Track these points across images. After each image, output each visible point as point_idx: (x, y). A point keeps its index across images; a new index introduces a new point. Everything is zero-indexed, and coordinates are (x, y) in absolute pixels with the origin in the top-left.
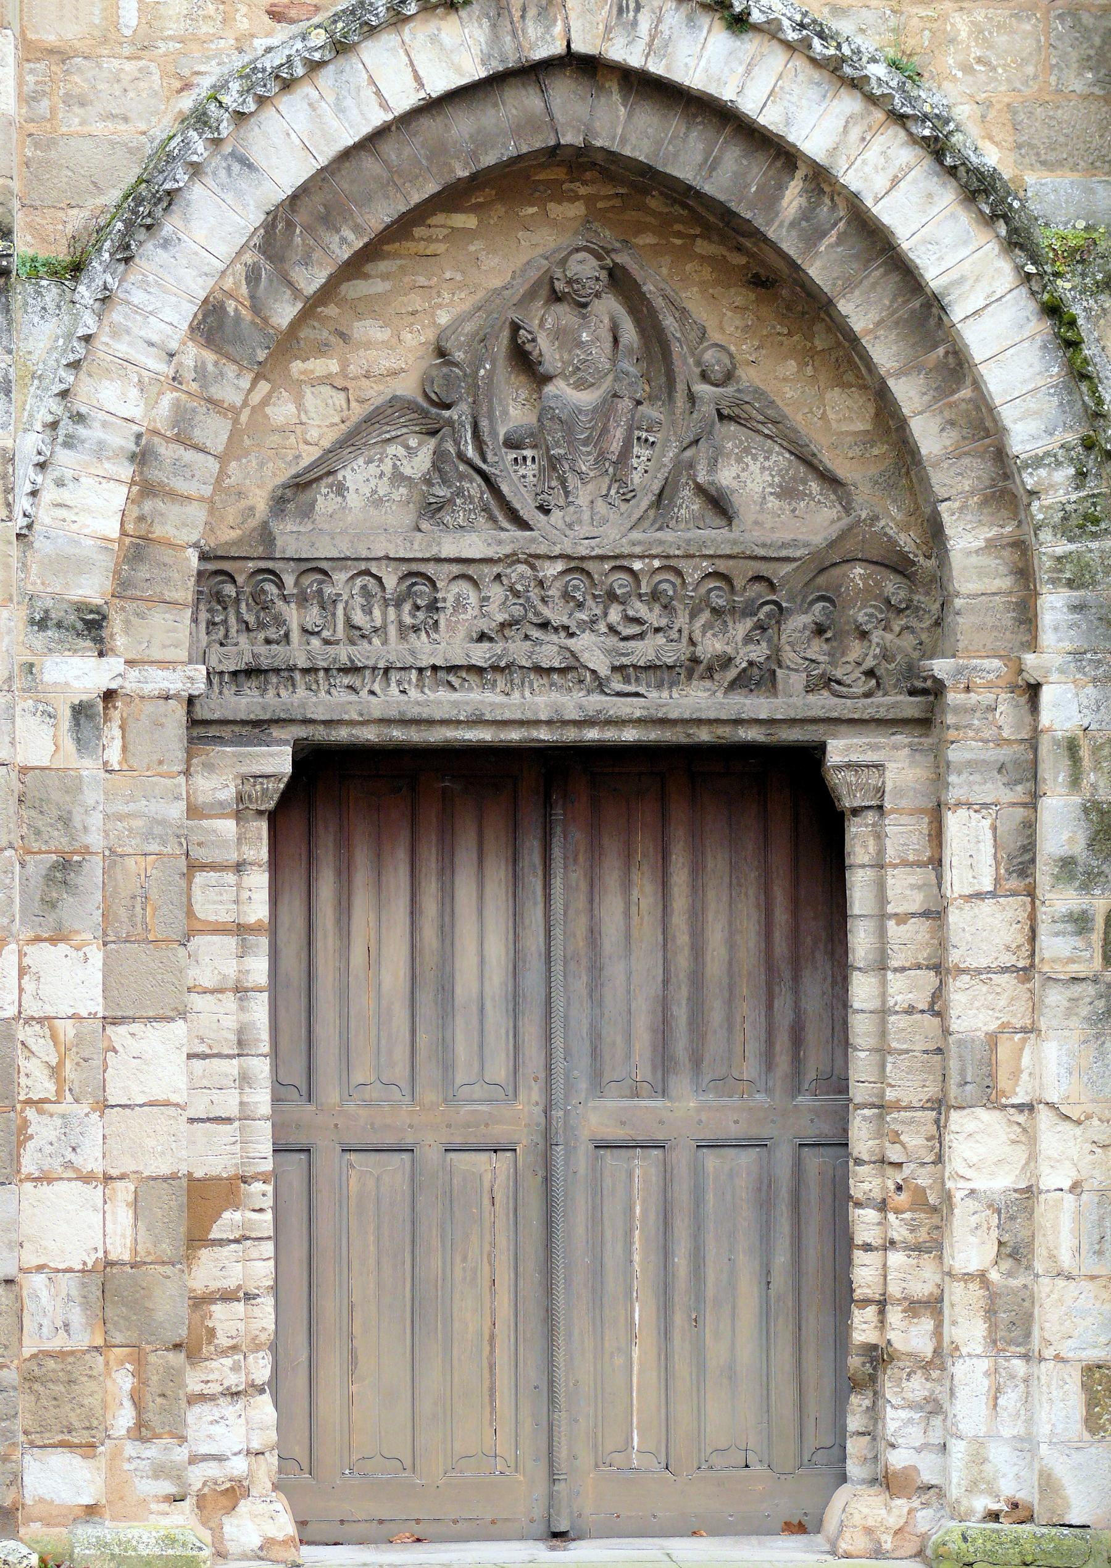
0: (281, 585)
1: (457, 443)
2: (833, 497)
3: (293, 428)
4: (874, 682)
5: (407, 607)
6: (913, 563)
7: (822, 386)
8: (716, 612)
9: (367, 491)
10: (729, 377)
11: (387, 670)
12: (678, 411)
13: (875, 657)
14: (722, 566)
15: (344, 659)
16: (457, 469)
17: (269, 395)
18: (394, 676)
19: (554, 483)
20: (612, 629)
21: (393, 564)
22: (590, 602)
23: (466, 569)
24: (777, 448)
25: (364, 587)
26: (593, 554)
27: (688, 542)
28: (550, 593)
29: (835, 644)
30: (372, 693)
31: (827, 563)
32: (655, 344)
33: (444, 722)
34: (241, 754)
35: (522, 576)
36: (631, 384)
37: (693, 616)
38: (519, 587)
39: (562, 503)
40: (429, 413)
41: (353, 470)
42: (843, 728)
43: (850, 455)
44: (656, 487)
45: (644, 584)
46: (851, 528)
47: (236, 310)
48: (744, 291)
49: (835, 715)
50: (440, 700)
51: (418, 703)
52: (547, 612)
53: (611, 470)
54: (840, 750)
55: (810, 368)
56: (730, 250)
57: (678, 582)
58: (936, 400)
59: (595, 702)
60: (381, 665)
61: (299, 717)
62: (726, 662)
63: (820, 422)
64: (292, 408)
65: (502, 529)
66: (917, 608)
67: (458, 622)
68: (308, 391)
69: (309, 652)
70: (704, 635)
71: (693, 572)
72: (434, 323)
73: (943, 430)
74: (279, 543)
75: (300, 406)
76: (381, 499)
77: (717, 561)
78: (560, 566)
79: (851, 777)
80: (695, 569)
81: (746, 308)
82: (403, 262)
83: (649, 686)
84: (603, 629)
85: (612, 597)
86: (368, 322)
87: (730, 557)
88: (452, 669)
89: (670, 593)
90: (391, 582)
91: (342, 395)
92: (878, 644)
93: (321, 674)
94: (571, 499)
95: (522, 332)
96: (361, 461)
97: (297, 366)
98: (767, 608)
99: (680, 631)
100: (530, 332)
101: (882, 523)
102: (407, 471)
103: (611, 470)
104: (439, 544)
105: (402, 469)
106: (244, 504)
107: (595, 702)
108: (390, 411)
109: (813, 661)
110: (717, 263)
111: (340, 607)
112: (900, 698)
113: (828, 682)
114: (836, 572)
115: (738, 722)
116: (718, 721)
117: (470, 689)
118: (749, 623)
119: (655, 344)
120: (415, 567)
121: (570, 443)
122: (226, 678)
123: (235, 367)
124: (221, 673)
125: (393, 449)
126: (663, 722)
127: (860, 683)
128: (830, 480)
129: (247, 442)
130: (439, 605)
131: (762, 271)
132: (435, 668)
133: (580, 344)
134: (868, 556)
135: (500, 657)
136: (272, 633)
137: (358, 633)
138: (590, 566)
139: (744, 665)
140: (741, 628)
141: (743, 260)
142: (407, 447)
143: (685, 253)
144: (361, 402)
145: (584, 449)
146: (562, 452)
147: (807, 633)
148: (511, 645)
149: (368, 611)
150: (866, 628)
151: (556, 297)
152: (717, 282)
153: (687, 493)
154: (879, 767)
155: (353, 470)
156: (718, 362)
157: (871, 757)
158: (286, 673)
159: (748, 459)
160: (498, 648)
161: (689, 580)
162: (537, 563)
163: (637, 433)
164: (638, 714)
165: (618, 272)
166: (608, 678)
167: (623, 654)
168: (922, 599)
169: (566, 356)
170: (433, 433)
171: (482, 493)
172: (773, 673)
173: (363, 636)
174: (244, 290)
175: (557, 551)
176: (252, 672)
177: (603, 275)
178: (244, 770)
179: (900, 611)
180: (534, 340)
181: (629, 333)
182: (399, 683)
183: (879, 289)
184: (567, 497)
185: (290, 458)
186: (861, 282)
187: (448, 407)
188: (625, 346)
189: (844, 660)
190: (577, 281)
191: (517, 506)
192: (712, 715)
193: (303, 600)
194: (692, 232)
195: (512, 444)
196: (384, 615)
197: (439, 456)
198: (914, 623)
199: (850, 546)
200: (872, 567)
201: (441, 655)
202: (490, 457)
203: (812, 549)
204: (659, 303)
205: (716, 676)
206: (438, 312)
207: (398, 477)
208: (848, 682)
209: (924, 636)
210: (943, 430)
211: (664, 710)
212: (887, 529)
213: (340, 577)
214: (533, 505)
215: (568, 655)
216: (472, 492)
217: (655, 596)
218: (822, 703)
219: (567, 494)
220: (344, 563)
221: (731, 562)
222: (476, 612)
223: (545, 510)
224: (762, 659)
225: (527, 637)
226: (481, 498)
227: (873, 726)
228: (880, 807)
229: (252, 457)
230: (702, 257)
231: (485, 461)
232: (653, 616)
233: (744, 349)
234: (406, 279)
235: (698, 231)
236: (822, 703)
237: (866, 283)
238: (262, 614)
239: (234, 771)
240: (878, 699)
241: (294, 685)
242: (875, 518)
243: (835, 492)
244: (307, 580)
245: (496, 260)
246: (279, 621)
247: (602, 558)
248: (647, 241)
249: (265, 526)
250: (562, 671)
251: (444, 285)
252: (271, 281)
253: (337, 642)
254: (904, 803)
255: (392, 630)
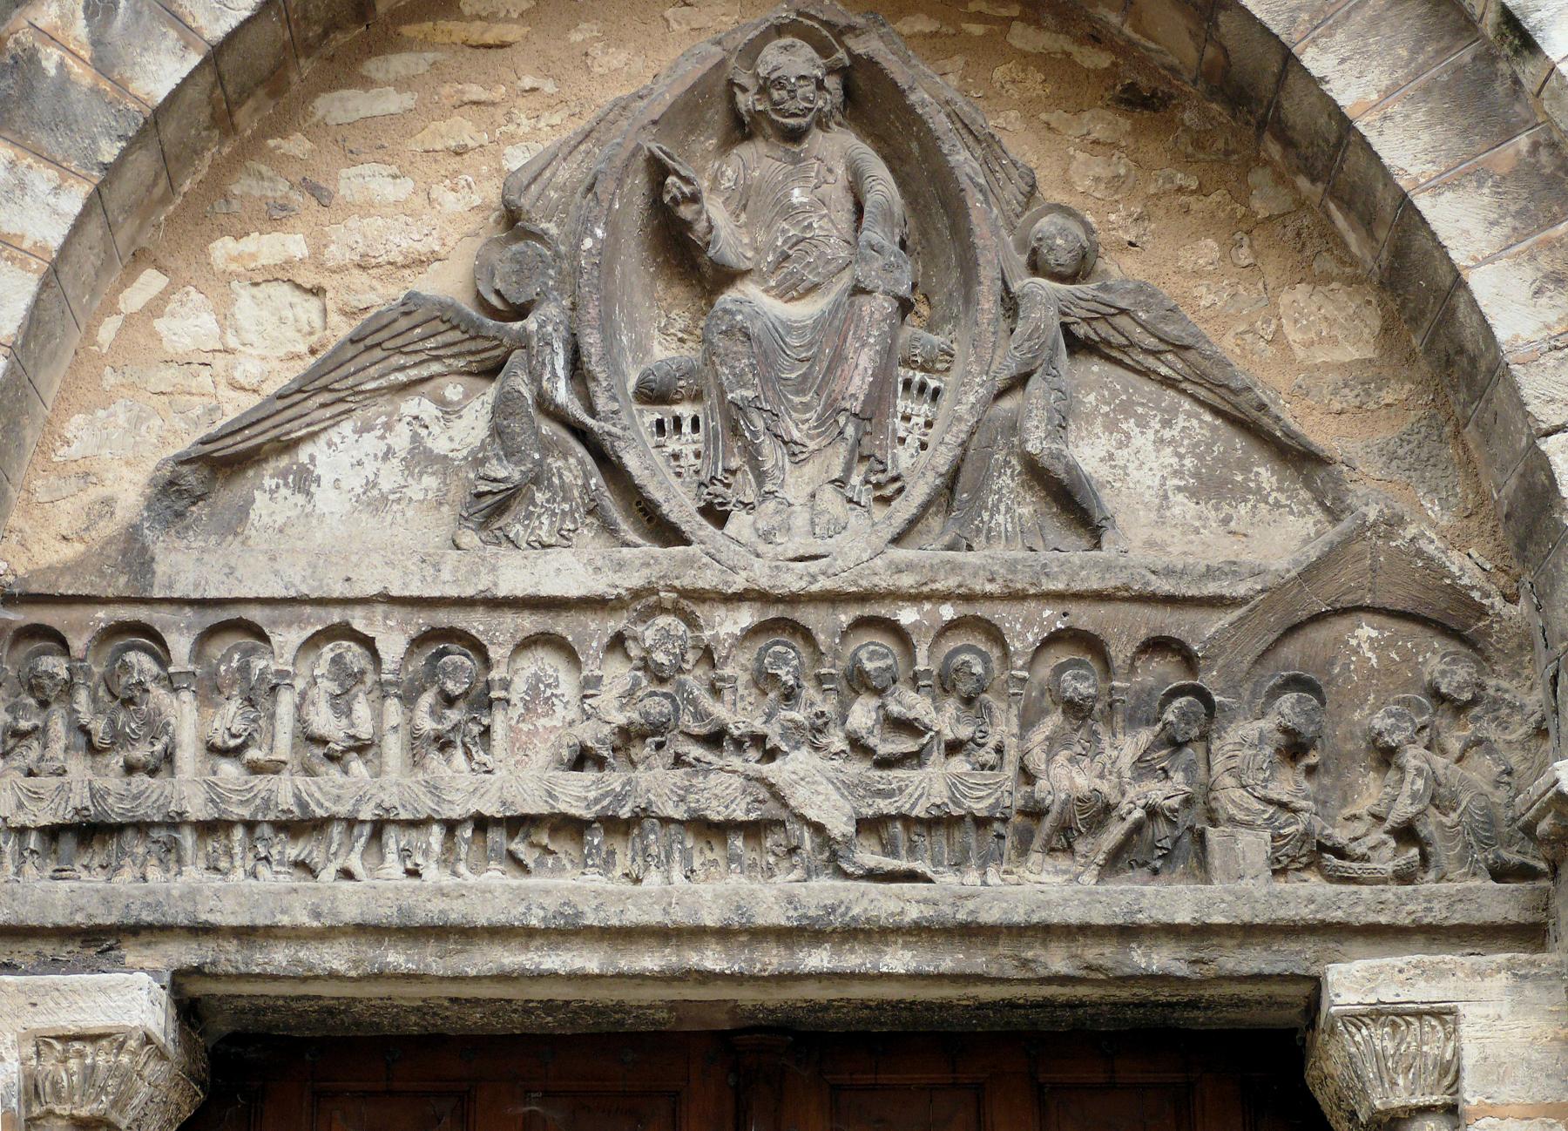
0: (162, 655)
1: (535, 378)
2: (1305, 494)
3: (208, 358)
4: (1414, 851)
5: (427, 699)
6: (1481, 612)
7: (1272, 283)
8: (1076, 710)
9: (357, 484)
10: (1080, 269)
11: (378, 828)
12: (984, 319)
13: (1414, 797)
14: (1085, 617)
15: (286, 800)
16: (537, 432)
17: (164, 297)
18: (393, 840)
19: (734, 463)
20: (858, 746)
21: (399, 613)
22: (809, 691)
23: (549, 619)
24: (1187, 405)
25: (337, 661)
26: (815, 588)
27: (1012, 566)
28: (727, 671)
29: (1327, 781)
30: (347, 874)
31: (1302, 615)
32: (934, 203)
33: (498, 933)
34: (34, 990)
35: (666, 635)
36: (889, 268)
37: (1027, 723)
38: (660, 657)
39: (750, 496)
40: (484, 338)
41: (330, 444)
42: (1357, 946)
43: (1337, 406)
44: (943, 459)
45: (922, 653)
46: (1347, 541)
47: (61, 65)
48: (1109, 115)
49: (1337, 915)
50: (487, 889)
51: (442, 892)
52: (720, 711)
53: (850, 431)
54: (1352, 981)
55: (1245, 251)
56: (1080, 41)
57: (995, 653)
58: (1519, 235)
59: (822, 893)
60: (366, 813)
61: (182, 920)
62: (1100, 812)
63: (1270, 351)
64: (208, 322)
65: (626, 544)
66: (1496, 703)
67: (534, 733)
68: (245, 298)
69: (212, 786)
70: (1049, 761)
71: (1024, 628)
72: (499, 170)
73: (1538, 293)
74: (161, 568)
75: (225, 319)
76: (384, 498)
77: (1073, 608)
78: (746, 617)
79: (1381, 1038)
80: (1028, 623)
81: (1114, 145)
82: (439, 56)
83: (936, 862)
84: (837, 742)
85: (858, 682)
86: (366, 169)
87: (1100, 597)
88: (518, 824)
89: (978, 669)
90: (393, 646)
91: (314, 304)
92: (1419, 772)
93: (238, 833)
94: (768, 487)
95: (671, 179)
96: (347, 427)
97: (223, 249)
98: (1181, 702)
99: (999, 750)
100: (687, 180)
101: (1412, 531)
102: (440, 446)
103: (850, 431)
104: (494, 569)
105: (429, 443)
106: (95, 493)
107: (822, 893)
108: (403, 323)
109: (1283, 806)
110: (1056, 67)
111: (286, 701)
112: (1477, 882)
113: (1318, 854)
114: (1320, 635)
115: (1128, 932)
116: (1084, 931)
117: (559, 869)
118: (1145, 736)
119: (934, 203)
120: (444, 618)
121: (765, 381)
122: (33, 841)
123: (52, 173)
124: (22, 831)
125: (412, 405)
126: (970, 932)
127: (1387, 852)
128: (1299, 458)
129: (110, 379)
130: (494, 694)
131: (1143, 81)
132: (482, 823)
133: (789, 212)
134: (1386, 601)
135: (620, 798)
136: (141, 752)
137: (320, 751)
138: (808, 616)
139: (1138, 814)
140: (1129, 746)
141: (1102, 60)
142: (442, 402)
143: (994, 48)
144: (349, 314)
145: (796, 400)
146: (750, 394)
147: (1268, 750)
148: (642, 776)
149: (341, 704)
150: (1393, 740)
151: (741, 129)
152: (1055, 102)
153: (1007, 481)
154: (1443, 1014)
155: (330, 444)
156: (1062, 232)
157: (1424, 992)
158: (162, 832)
159: (1129, 425)
160: (615, 780)
161: (1015, 645)
162: (700, 611)
163: (903, 373)
164: (913, 913)
165: (861, 81)
166: (848, 842)
167: (880, 793)
168: (1504, 684)
169: (761, 237)
170: (491, 372)
171: (587, 476)
172: (1201, 838)
173: (331, 758)
174: (80, 29)
175: (739, 583)
176: (90, 832)
177: (832, 83)
178: (44, 1021)
179: (1460, 709)
180: (695, 198)
181: (882, 186)
182: (405, 854)
183: (1385, 29)
184: (760, 484)
185: (199, 411)
186: (1348, 15)
187: (521, 312)
188: (877, 205)
189: (1347, 812)
190: (779, 83)
191: (657, 495)
192: (1074, 916)
193: (210, 691)
194: (1004, 12)
195: (653, 393)
196: (378, 716)
197: (504, 407)
198: (1491, 732)
199: (1346, 582)
200: (1395, 626)
201: (494, 793)
202: (602, 403)
203: (1270, 580)
204: (940, 122)
205: (1080, 846)
206: (508, 150)
207: (421, 458)
208: (1360, 849)
209: (1514, 759)
210: (1538, 293)
211: (970, 905)
212: (1423, 544)
213: (288, 639)
214: (692, 506)
215: (763, 794)
216: (568, 477)
217: (945, 683)
218: (1309, 895)
219: (761, 477)
220: (296, 610)
221: (1103, 610)
222: (573, 713)
223: (716, 515)
224: (1174, 803)
225: (679, 761)
226: (586, 486)
227: (1420, 940)
228: (1451, 1110)
229: (119, 408)
230: (1025, 55)
231: (593, 412)
232: (946, 720)
233: (1114, 223)
234: (446, 90)
235: (1015, 10)
236: (1309, 895)
237: (1357, 18)
238: (122, 717)
239: (18, 1024)
240: (1427, 884)
241: (180, 861)
242: (1394, 522)
243: (1308, 485)
244: (217, 649)
245: (623, 56)
246: (155, 727)
247: (833, 599)
248: (918, 27)
249: (133, 533)
250: (754, 830)
251: (521, 102)
252: (138, 13)
253: (275, 768)
254: (1506, 1093)
255: (394, 747)
